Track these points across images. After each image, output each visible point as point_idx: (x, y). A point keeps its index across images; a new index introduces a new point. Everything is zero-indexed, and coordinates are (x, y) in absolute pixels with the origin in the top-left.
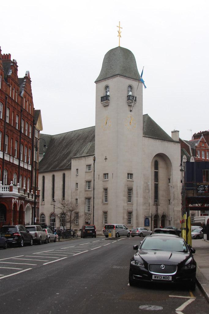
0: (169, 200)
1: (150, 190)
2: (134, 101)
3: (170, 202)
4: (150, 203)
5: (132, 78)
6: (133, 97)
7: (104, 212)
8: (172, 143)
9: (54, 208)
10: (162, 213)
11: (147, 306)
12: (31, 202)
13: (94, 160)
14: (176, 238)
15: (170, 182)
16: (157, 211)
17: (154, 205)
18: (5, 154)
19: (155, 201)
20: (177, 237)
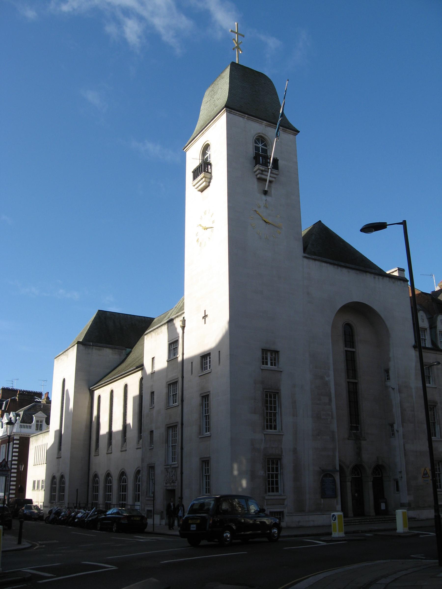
0: (392, 425)
1: (333, 395)
3: (393, 430)
7: (203, 461)
15: (388, 379)
16: (359, 453)
17: (348, 439)
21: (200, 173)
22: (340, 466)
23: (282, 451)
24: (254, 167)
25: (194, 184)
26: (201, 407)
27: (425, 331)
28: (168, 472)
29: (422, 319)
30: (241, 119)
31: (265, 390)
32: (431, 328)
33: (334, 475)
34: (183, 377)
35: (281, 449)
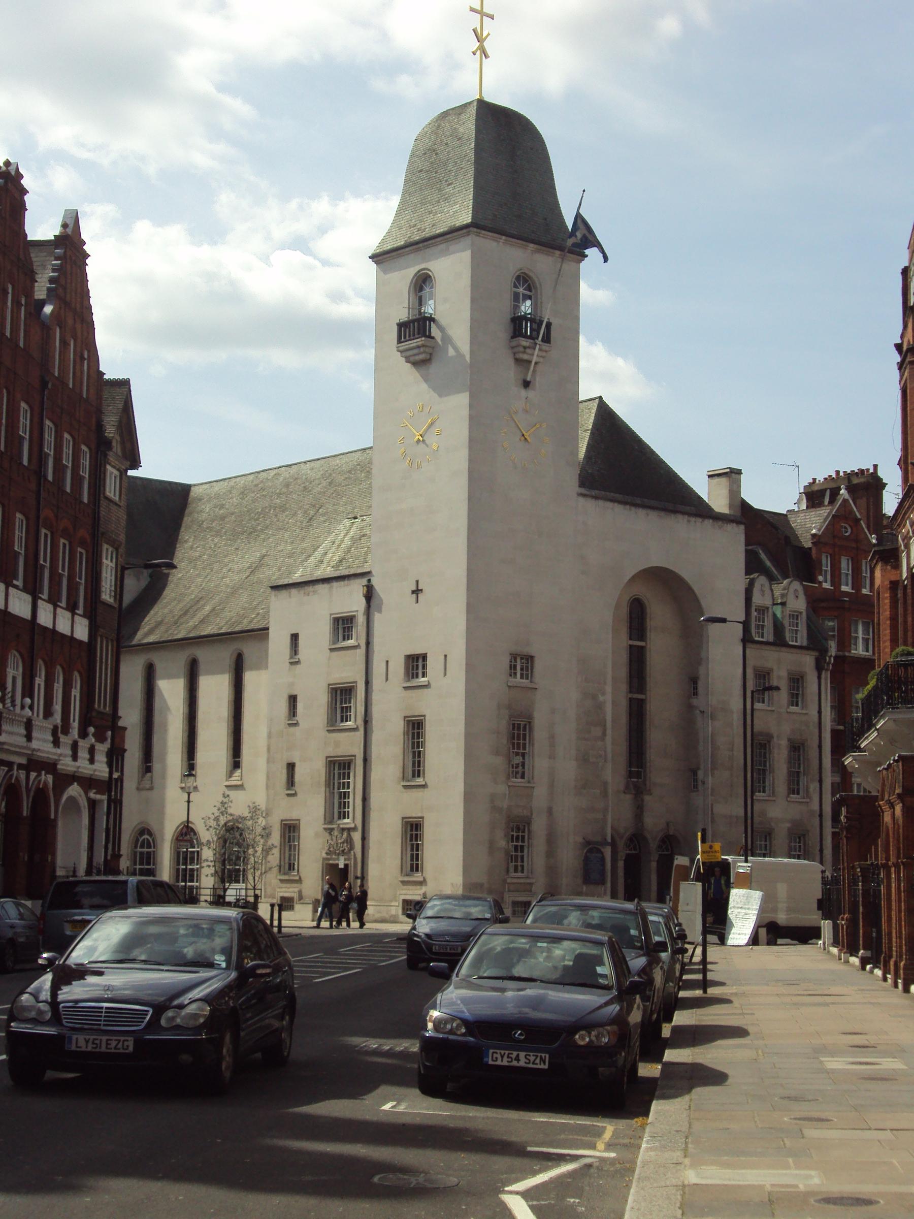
0: (694, 772)
1: (609, 724)
2: (543, 340)
3: (696, 780)
4: (605, 784)
6: (535, 326)
8: (708, 523)
9: (189, 802)
11: (910, 597)
12: (88, 783)
14: (41, 748)
15: (696, 694)
17: (624, 793)
18: (40, 602)
19: (630, 775)
20: (39, 750)
23: (532, 814)
30: (494, 244)
33: (603, 850)
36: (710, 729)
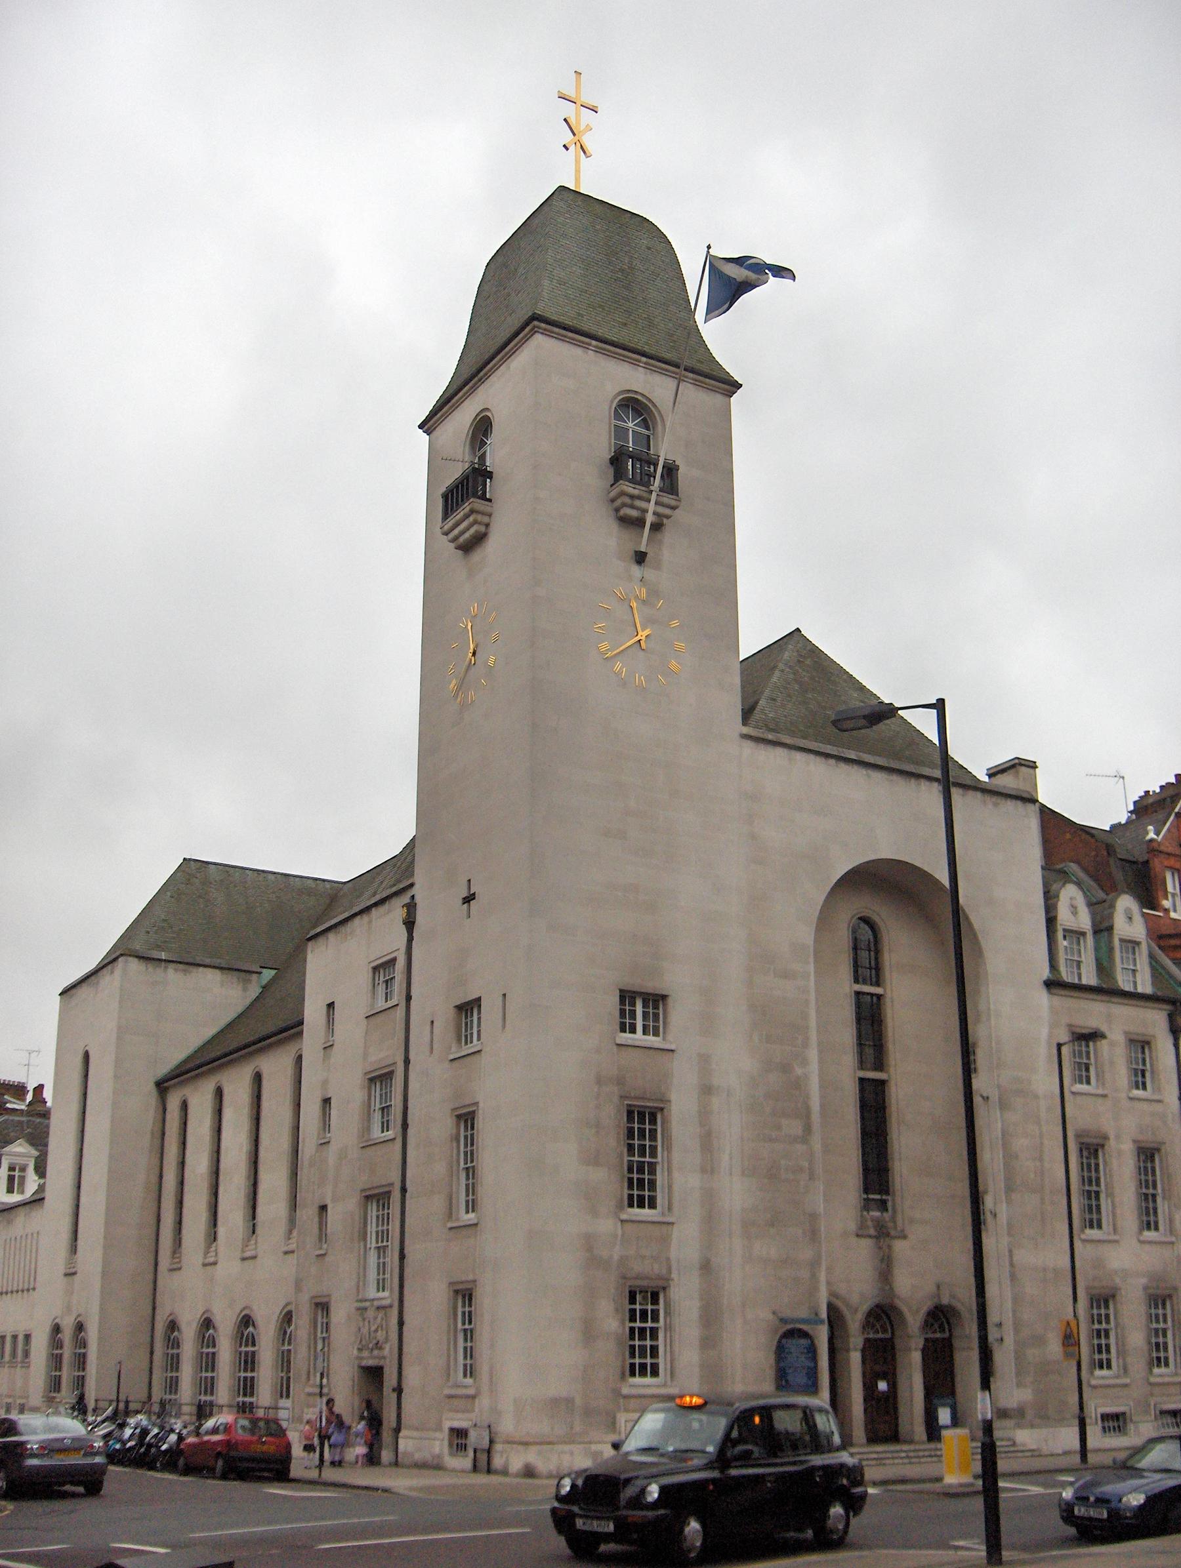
5: (644, 354)
7: (457, 1292)
10: (930, 1288)
13: (410, 924)
16: (885, 1274)
21: (462, 500)
22: (831, 1307)
24: (612, 486)
25: (446, 528)
26: (455, 1144)
27: (1082, 938)
28: (364, 1319)
29: (1072, 906)
31: (626, 1102)
32: (1097, 931)
34: (407, 1061)
35: (668, 1259)
36: (999, 1125)
